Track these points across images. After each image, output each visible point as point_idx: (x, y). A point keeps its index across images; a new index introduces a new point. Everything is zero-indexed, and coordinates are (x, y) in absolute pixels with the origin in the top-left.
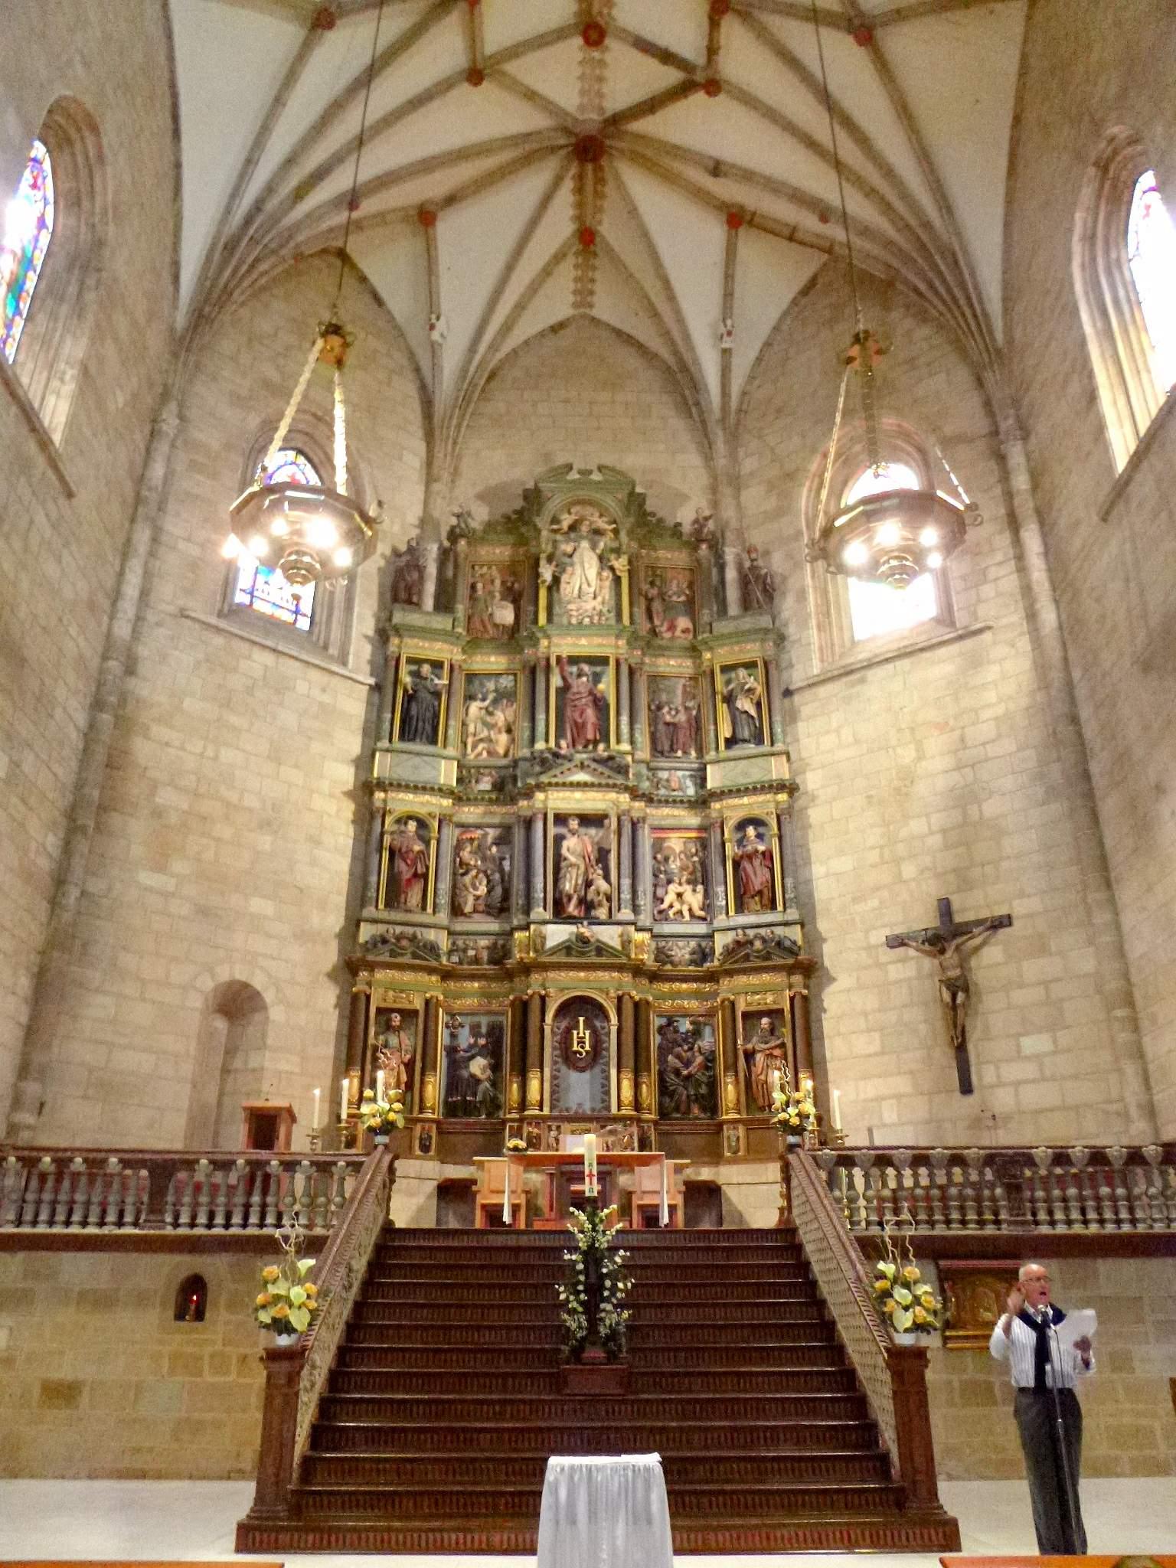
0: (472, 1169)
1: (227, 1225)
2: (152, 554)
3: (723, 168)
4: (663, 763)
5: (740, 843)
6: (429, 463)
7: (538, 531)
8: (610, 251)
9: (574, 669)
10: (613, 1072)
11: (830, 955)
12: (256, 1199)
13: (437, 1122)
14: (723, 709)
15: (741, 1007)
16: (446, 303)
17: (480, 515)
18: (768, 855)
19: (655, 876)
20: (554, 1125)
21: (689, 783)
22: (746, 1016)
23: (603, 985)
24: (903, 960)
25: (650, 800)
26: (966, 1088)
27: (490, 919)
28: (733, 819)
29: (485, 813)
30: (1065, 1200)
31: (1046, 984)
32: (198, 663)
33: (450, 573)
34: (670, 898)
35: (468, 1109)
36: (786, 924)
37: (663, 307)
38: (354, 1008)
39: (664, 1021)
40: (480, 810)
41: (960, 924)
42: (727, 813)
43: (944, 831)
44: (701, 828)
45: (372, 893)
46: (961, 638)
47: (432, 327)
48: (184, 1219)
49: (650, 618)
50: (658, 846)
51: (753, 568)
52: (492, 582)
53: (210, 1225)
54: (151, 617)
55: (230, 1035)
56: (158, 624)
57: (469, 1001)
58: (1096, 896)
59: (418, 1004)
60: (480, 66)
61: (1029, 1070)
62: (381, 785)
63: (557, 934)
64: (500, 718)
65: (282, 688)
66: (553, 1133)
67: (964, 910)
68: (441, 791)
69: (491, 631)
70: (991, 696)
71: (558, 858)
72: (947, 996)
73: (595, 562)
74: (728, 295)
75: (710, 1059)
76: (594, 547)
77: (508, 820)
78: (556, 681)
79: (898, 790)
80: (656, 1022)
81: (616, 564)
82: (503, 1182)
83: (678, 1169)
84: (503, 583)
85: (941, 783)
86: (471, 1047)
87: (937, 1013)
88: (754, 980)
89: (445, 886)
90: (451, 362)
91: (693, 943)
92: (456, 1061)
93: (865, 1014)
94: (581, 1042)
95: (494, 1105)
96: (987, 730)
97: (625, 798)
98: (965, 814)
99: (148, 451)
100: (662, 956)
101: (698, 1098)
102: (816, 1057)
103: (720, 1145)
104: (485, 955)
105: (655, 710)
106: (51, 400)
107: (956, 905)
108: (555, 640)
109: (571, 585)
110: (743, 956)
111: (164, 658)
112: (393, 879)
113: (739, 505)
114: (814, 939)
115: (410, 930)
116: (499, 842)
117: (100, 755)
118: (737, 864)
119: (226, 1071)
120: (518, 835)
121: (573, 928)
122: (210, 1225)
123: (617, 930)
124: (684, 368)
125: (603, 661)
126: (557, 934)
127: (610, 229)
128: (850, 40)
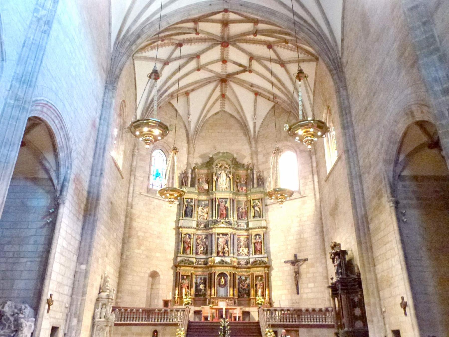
1: (161, 321)
4: (239, 221)
5: (255, 239)
6: (188, 149)
8: (229, 99)
9: (221, 200)
12: (166, 316)
13: (194, 299)
14: (252, 209)
16: (192, 112)
17: (200, 161)
18: (261, 242)
22: (256, 276)
23: (227, 270)
24: (288, 266)
28: (254, 234)
31: (314, 273)
33: (194, 176)
34: (241, 251)
35: (200, 295)
36: (264, 257)
37: (240, 111)
38: (177, 275)
39: (239, 277)
40: (202, 231)
42: (253, 233)
43: (296, 240)
44: (247, 235)
45: (180, 251)
47: (189, 118)
50: (238, 239)
51: (259, 176)
54: (135, 195)
56: (136, 197)
57: (200, 273)
59: (190, 274)
60: (199, 67)
61: (309, 290)
62: (181, 227)
63: (218, 259)
64: (205, 210)
69: (203, 191)
71: (218, 243)
72: (295, 275)
74: (255, 110)
75: (249, 285)
76: (225, 171)
77: (208, 234)
78: (217, 203)
80: (238, 277)
81: (229, 176)
82: (207, 310)
83: (241, 309)
84: (205, 179)
86: (200, 283)
88: (258, 269)
89: (194, 249)
90: (193, 125)
91: (245, 260)
92: (197, 286)
94: (222, 282)
95: (205, 295)
97: (232, 230)
98: (300, 236)
100: (239, 263)
101: (246, 293)
104: (203, 263)
105: (238, 209)
107: (298, 255)
108: (217, 194)
110: (255, 264)
111: (138, 204)
112: (184, 248)
113: (257, 159)
116: (205, 238)
118: (254, 244)
119: (152, 288)
120: (209, 237)
122: (158, 321)
125: (227, 199)
126: (218, 259)
127: (228, 93)
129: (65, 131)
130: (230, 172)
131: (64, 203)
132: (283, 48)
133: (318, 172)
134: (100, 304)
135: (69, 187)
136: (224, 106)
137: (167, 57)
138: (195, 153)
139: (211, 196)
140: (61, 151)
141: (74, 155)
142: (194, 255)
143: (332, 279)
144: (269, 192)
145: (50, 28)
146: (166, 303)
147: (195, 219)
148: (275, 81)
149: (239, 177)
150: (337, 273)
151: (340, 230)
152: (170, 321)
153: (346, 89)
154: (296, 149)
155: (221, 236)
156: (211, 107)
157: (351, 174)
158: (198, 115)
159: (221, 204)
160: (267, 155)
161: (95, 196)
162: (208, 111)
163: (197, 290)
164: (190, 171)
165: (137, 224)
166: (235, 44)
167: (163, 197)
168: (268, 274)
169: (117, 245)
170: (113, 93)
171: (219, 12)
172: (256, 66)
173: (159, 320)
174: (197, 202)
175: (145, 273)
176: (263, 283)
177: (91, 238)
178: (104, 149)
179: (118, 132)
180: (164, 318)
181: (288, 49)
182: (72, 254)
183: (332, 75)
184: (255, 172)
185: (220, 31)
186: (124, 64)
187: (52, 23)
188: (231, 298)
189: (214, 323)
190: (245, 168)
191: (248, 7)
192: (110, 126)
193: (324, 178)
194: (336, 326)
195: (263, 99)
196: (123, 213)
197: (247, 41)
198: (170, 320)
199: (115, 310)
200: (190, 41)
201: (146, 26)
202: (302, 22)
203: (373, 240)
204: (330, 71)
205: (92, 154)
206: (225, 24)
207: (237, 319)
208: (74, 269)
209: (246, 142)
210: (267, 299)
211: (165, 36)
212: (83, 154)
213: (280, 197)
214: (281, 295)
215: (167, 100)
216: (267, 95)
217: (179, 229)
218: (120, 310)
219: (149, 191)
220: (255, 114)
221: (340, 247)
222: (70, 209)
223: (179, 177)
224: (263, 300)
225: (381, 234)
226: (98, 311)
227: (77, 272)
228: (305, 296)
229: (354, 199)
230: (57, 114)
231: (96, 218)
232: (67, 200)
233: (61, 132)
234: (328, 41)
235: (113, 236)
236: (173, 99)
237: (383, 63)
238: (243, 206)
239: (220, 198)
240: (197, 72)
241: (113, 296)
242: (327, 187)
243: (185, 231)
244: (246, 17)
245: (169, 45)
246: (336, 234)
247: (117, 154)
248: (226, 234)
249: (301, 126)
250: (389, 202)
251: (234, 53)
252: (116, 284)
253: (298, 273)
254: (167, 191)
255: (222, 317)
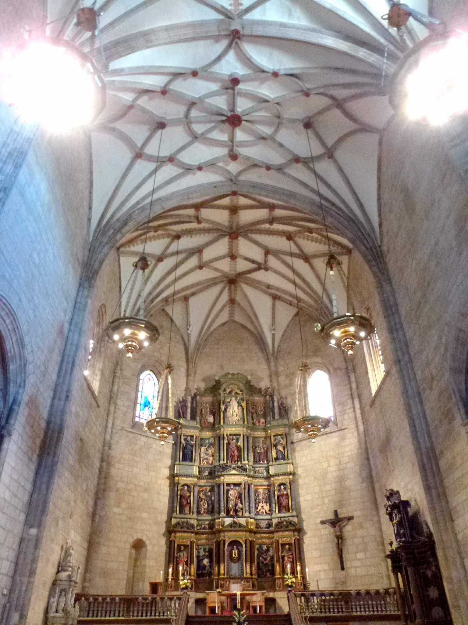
0: (205, 594)
1: (146, 616)
2: (114, 412)
3: (270, 287)
6: (188, 370)
7: (220, 394)
8: (239, 305)
9: (231, 437)
10: (244, 563)
11: (306, 526)
12: (154, 608)
13: (194, 580)
14: (273, 448)
15: (280, 542)
16: (192, 320)
17: (202, 386)
18: (287, 495)
19: (255, 501)
20: (228, 580)
21: (265, 471)
22: (282, 544)
23: (241, 537)
24: (326, 528)
25: (253, 477)
26: (343, 568)
27: (208, 515)
28: (277, 483)
29: (207, 482)
30: (355, 606)
31: (363, 537)
32: (127, 443)
33: (194, 405)
34: (260, 507)
36: (292, 516)
38: (170, 544)
40: (205, 481)
41: (341, 518)
43: (335, 489)
44: (268, 486)
45: (175, 509)
46: (339, 430)
47: (188, 329)
48: (135, 615)
49: (253, 420)
50: (256, 491)
51: (282, 404)
52: (207, 408)
53: (142, 616)
54: (114, 431)
55: (136, 554)
56: (116, 433)
58: (374, 513)
59: (189, 543)
60: (202, 265)
62: (177, 476)
63: (228, 521)
64: (210, 452)
65: (149, 447)
66: (228, 583)
67: (341, 514)
68: (194, 476)
70: (347, 449)
72: (336, 541)
73: (237, 403)
74: (273, 318)
75: (272, 558)
76: (236, 398)
77: (213, 484)
78: (226, 441)
79: (323, 476)
80: (257, 546)
82: (214, 598)
83: (263, 594)
84: (210, 409)
85: (335, 474)
86: (203, 556)
87: (334, 545)
88: (284, 533)
89: (195, 506)
91: (266, 522)
92: (200, 561)
93: (315, 544)
94: (235, 554)
95: (210, 574)
96: (346, 459)
97: (246, 478)
99: (113, 382)
100: (258, 526)
101: (269, 571)
102: (302, 558)
103: (275, 585)
104: (207, 526)
105: (255, 448)
106: (95, 382)
107: (339, 512)
108: (225, 429)
109: (230, 411)
110: (281, 526)
111: (118, 442)
113: (278, 381)
114: (300, 521)
115: (186, 520)
116: (210, 491)
117: (103, 475)
118: (278, 497)
119: (135, 566)
120: (216, 489)
121: (232, 519)
123: (244, 519)
124: (262, 339)
125: (240, 435)
126: (228, 521)
127: (239, 298)
128: (302, 261)
129: (19, 335)
130: (242, 400)
131: (10, 435)
132: (306, 240)
133: (359, 396)
134: (57, 590)
135: (19, 412)
136: (234, 314)
137: (161, 252)
138: (197, 375)
139: (218, 431)
140: (12, 362)
141: (30, 368)
142: (195, 516)
143: (391, 544)
144: (295, 422)
145: (7, 196)
146: (154, 587)
147: (197, 464)
148: (298, 280)
149: (254, 405)
150: (398, 535)
151: (396, 472)
152: (159, 616)
153: (390, 283)
154: (328, 366)
155: (232, 486)
156: (217, 316)
157: (407, 392)
158: (199, 327)
159: (231, 442)
160: (291, 376)
161: (57, 427)
162: (213, 321)
163: (200, 567)
164: (189, 399)
165: (118, 471)
166: (247, 235)
167: (153, 431)
168: (299, 540)
169: (87, 502)
170: (89, 291)
171: (227, 196)
172: (273, 262)
173: (144, 614)
174: (198, 440)
175: (125, 542)
176: (292, 554)
177: (48, 488)
178: (73, 363)
179: (94, 344)
180: (151, 610)
181: (312, 241)
182: (18, 512)
183: (371, 267)
184: (275, 399)
185: (227, 220)
186: (106, 256)
187: (10, 190)
188: (248, 578)
189: (225, 616)
190: (263, 393)
191: (261, 189)
192: (82, 334)
193: (369, 403)
194: (402, 617)
195: (284, 304)
196: (98, 456)
197: (261, 232)
198: (159, 613)
199: (81, 599)
200: (190, 232)
201: (134, 212)
202: (328, 205)
203: (447, 482)
204: (368, 262)
205: (57, 369)
206: (234, 210)
207: (258, 611)
208: (20, 535)
209: (262, 360)
210: (299, 578)
211: (159, 226)
212: (43, 368)
213: (312, 429)
214: (318, 571)
215: (160, 305)
216: (290, 299)
217: (174, 478)
218: (87, 599)
219: (135, 425)
220: (273, 323)
221: (399, 496)
222: (20, 444)
223: (175, 407)
224: (294, 580)
225: (457, 474)
226: (54, 600)
227: (24, 539)
228: (352, 572)
229: (413, 426)
230: (10, 311)
231: (56, 459)
232: (15, 431)
233: (13, 335)
234: (364, 227)
235: (82, 488)
236: (168, 305)
237: (437, 244)
238: (261, 445)
239: (230, 435)
240: (198, 271)
241: (78, 577)
242: (373, 414)
243: (183, 480)
244: (259, 201)
245: (163, 238)
246: (390, 479)
247: (91, 375)
248: (239, 485)
249: (339, 324)
250: (464, 426)
251: (245, 247)
252: (83, 559)
253: (342, 538)
254: (157, 422)
255: (235, 608)
